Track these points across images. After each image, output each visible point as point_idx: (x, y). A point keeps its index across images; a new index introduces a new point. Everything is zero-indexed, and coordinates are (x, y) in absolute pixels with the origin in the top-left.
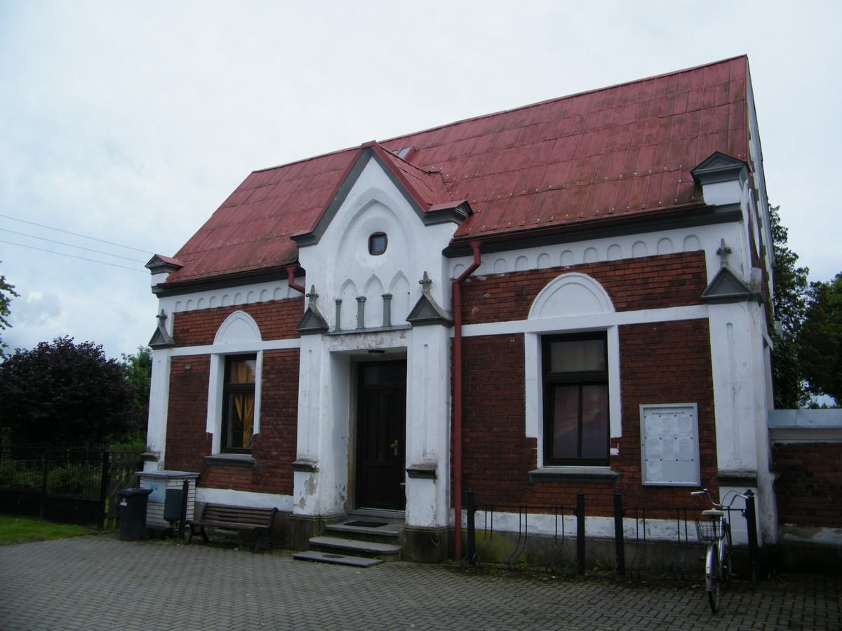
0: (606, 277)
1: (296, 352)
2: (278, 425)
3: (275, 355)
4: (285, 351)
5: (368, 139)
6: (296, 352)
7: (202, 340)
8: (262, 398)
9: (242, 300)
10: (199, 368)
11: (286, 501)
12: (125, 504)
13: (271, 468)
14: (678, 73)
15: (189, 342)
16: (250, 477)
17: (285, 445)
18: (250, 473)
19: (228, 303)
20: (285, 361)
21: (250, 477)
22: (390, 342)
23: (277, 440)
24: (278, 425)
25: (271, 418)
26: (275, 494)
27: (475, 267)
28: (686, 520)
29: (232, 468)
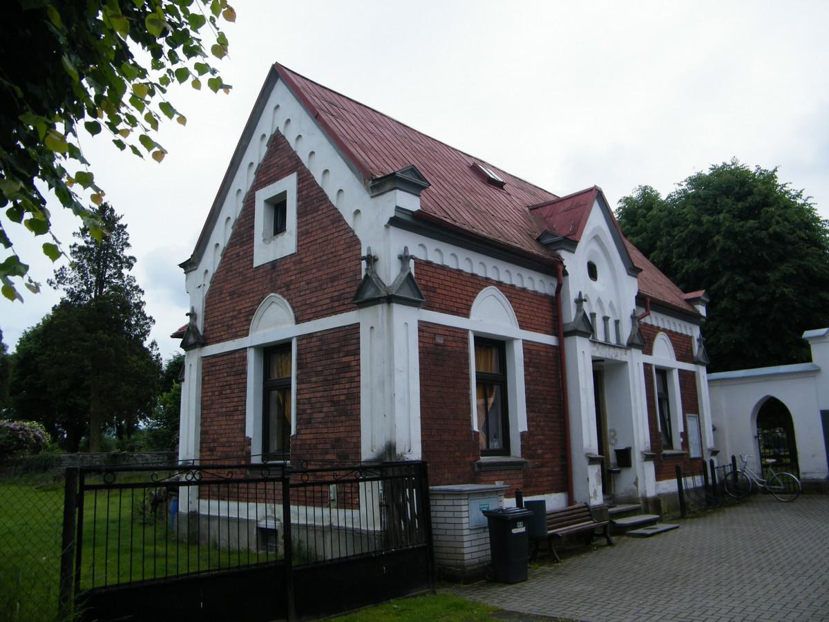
0: (427, 291)
1: (355, 328)
2: (540, 422)
3: (531, 348)
4: (537, 344)
5: (234, 8)
6: (355, 328)
7: (455, 309)
8: (244, 390)
9: (505, 279)
10: (454, 344)
11: (555, 499)
12: (523, 529)
13: (538, 467)
14: (572, 197)
15: (437, 305)
16: (522, 481)
17: (547, 442)
18: (521, 476)
19: (492, 275)
20: (539, 355)
21: (522, 481)
22: (620, 356)
23: (541, 437)
24: (540, 422)
25: (534, 414)
26: (543, 494)
27: (643, 316)
28: (338, 526)
29: (503, 473)
